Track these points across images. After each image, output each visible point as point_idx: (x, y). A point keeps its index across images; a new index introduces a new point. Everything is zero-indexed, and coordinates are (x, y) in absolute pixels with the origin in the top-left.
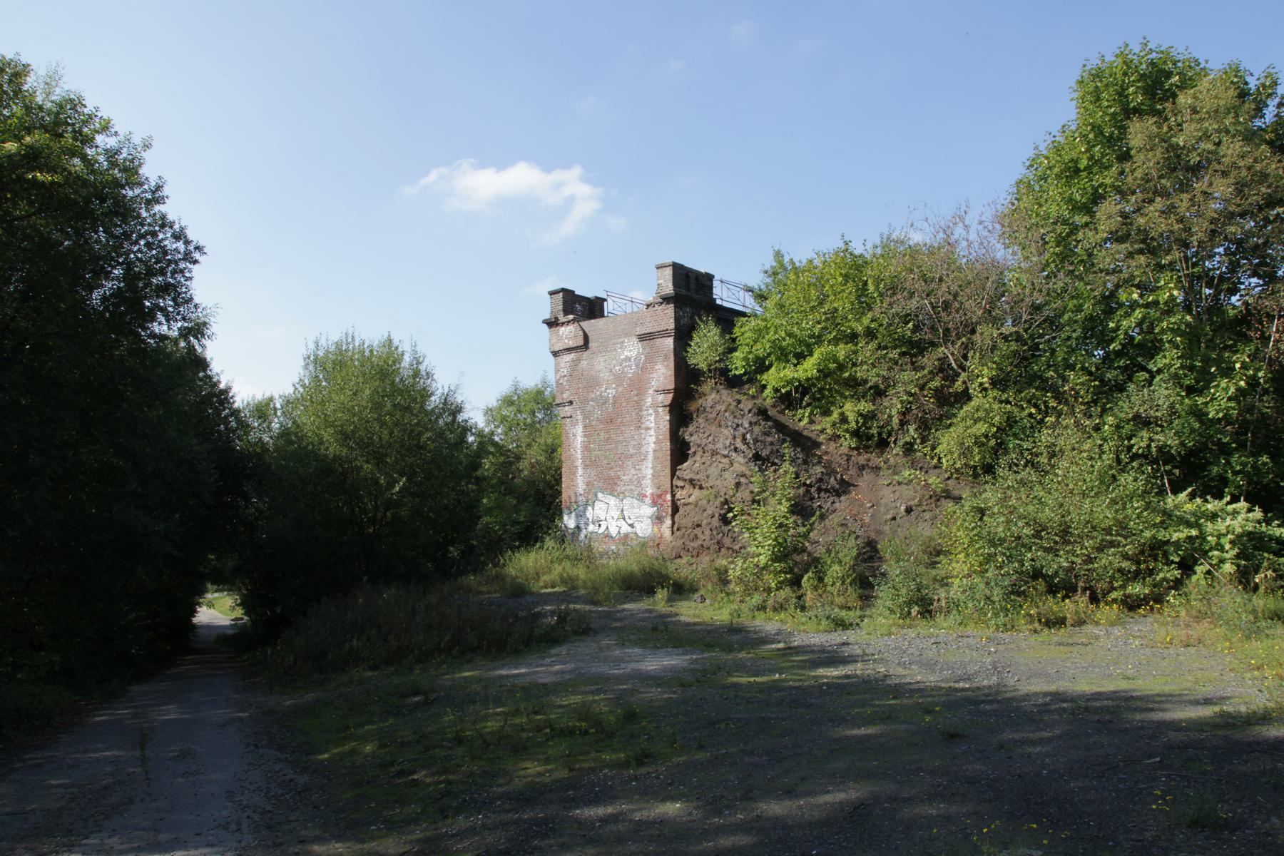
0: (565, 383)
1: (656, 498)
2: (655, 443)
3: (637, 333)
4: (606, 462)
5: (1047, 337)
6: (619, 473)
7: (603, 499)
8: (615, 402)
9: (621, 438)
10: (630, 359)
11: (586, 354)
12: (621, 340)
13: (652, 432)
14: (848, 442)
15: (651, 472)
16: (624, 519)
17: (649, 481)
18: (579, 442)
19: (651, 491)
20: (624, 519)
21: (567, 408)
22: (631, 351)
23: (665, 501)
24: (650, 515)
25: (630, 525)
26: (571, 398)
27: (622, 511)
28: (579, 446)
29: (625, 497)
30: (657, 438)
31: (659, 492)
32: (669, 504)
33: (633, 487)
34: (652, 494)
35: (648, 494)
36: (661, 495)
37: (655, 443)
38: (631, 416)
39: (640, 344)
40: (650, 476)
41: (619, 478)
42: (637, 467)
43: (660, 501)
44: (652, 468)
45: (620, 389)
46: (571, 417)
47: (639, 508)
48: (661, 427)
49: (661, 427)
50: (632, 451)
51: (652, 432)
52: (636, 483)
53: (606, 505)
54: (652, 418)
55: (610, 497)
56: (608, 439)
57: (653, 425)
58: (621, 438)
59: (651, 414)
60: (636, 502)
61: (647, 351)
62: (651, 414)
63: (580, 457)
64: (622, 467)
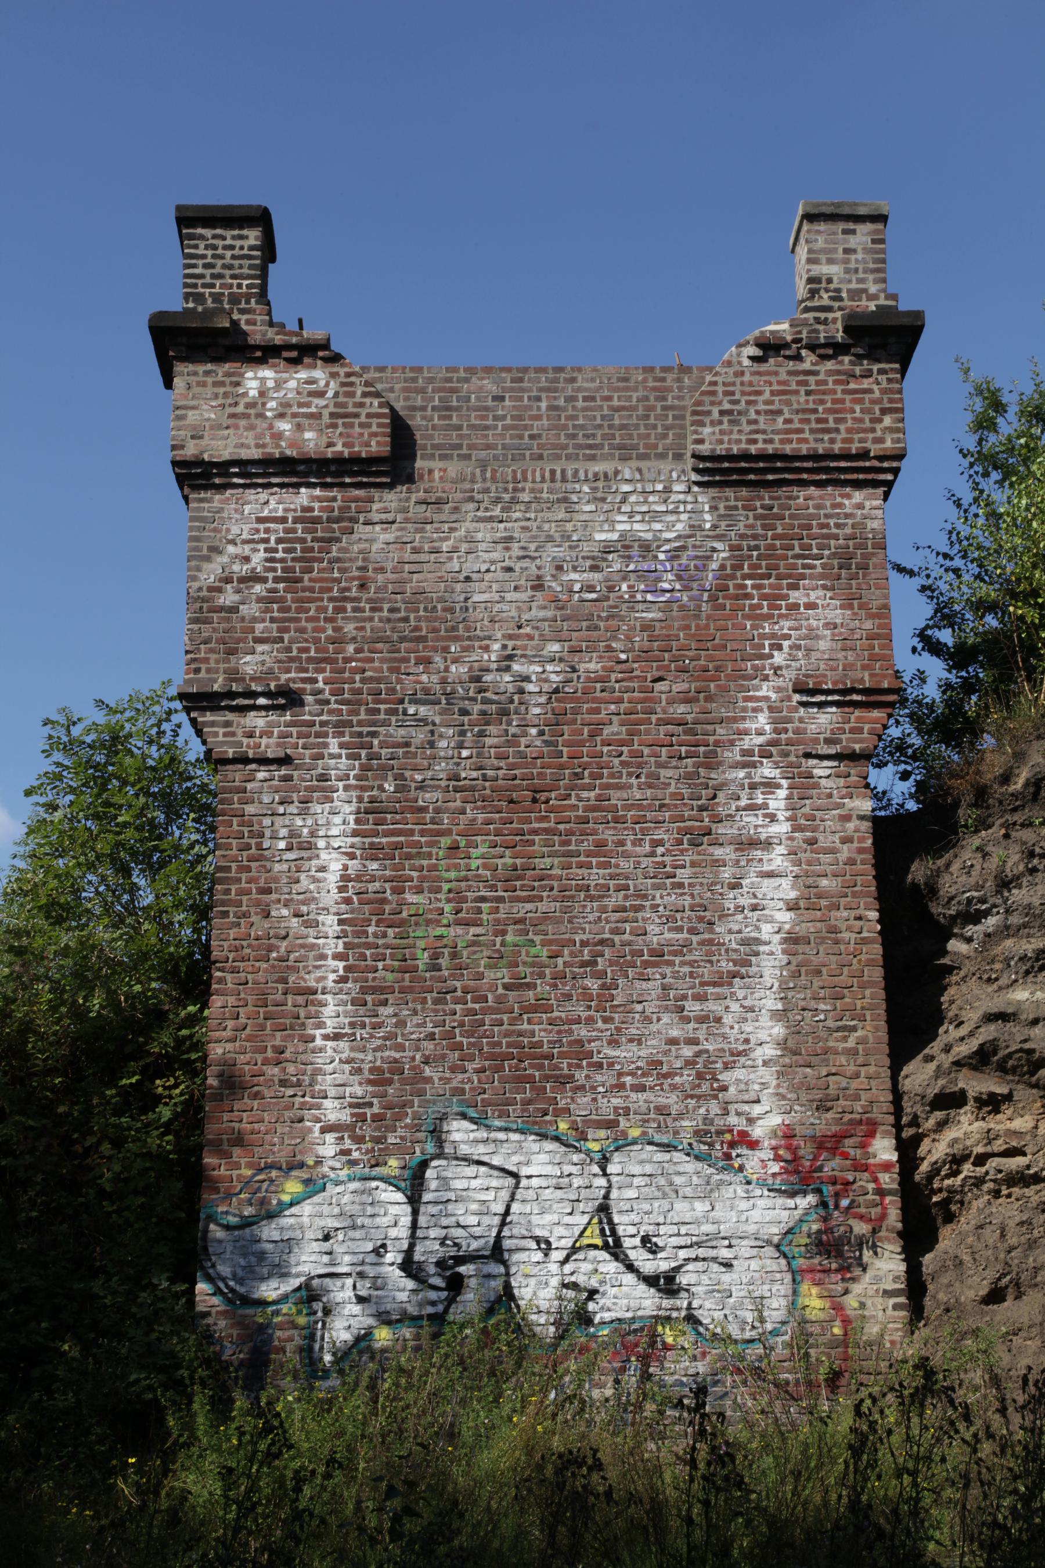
0: (247, 610)
1: (806, 1151)
2: (792, 907)
3: (705, 449)
4: (503, 975)
5: (182, 1087)
6: (582, 1032)
7: (480, 1151)
8: (556, 721)
9: (596, 876)
10: (647, 548)
11: (391, 499)
12: (598, 467)
13: (777, 859)
14: (637, 1241)
15: (779, 1030)
16: (615, 1249)
17: (768, 1075)
18: (332, 878)
19: (775, 1120)
20: (615, 1249)
21: (257, 721)
22: (654, 516)
23: (861, 1167)
24: (775, 1231)
25: (651, 1281)
26: (290, 677)
27: (604, 1209)
28: (330, 894)
29: (622, 1143)
30: (806, 880)
31: (824, 1124)
32: (889, 1180)
33: (671, 1100)
34: (788, 1134)
35: (757, 1132)
36: (839, 1137)
37: (792, 907)
38: (653, 781)
39: (704, 498)
40: (769, 1051)
41: (580, 1052)
42: (693, 1007)
43: (832, 1166)
44: (778, 1016)
45: (592, 666)
46: (285, 761)
47: (708, 1191)
48: (824, 841)
49: (824, 841)
50: (657, 934)
51: (777, 859)
52: (686, 1078)
53: (510, 1181)
54: (778, 801)
55: (531, 1142)
56: (515, 873)
57: (782, 828)
58: (596, 876)
59: (770, 786)
60: (691, 1166)
61: (743, 522)
62: (770, 786)
63: (333, 946)
64: (604, 999)
